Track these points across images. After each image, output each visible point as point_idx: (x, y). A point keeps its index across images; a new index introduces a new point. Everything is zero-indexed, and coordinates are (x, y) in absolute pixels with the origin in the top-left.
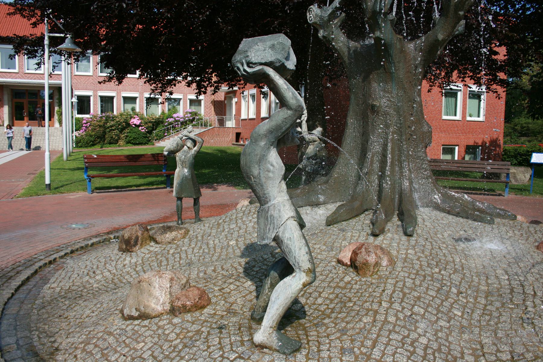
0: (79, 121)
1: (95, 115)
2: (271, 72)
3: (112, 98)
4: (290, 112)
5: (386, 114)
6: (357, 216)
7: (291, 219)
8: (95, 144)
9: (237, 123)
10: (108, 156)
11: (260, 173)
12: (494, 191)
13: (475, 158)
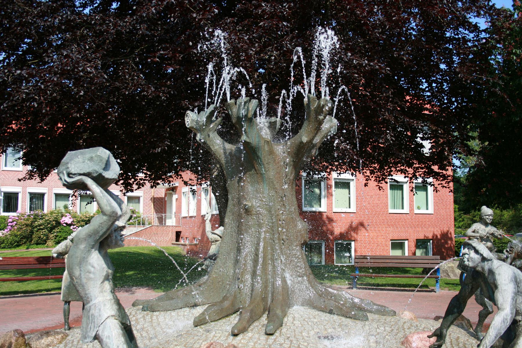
0: (5, 219)
1: (23, 213)
2: (89, 182)
3: (42, 195)
4: (105, 218)
5: (258, 214)
6: (227, 316)
7: (111, 318)
8: (21, 245)
9: (178, 221)
10: (15, 258)
11: (80, 274)
12: (426, 286)
13: (427, 253)
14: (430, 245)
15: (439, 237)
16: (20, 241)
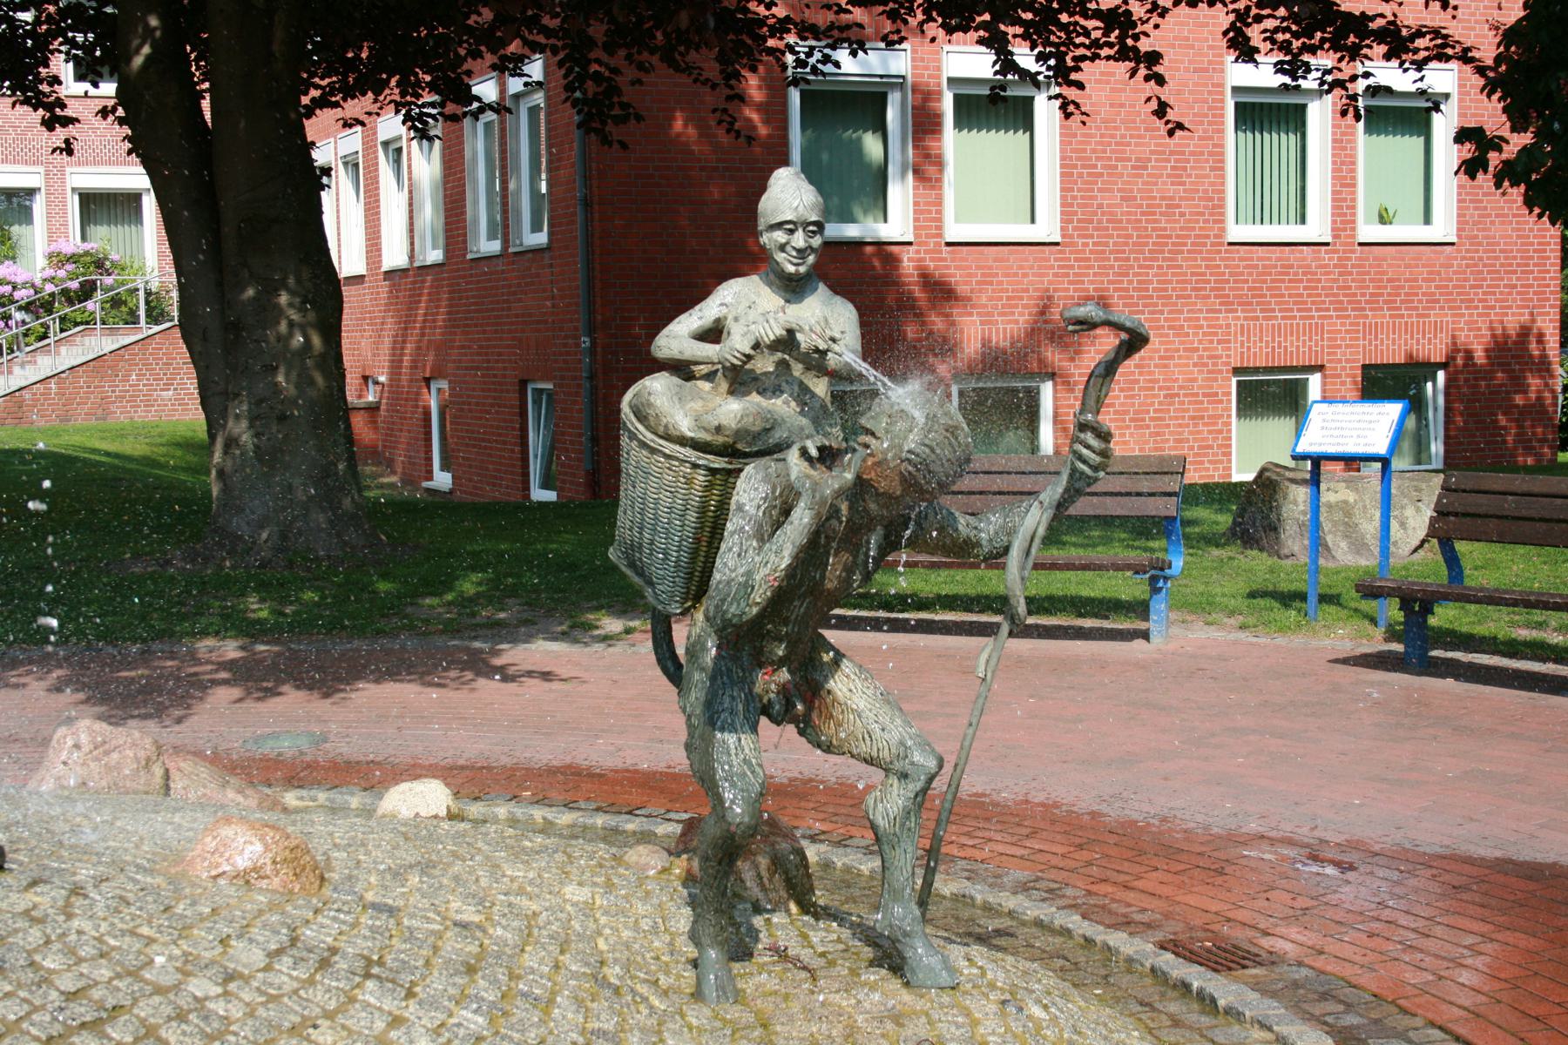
14: (1436, 388)
15: (1479, 356)
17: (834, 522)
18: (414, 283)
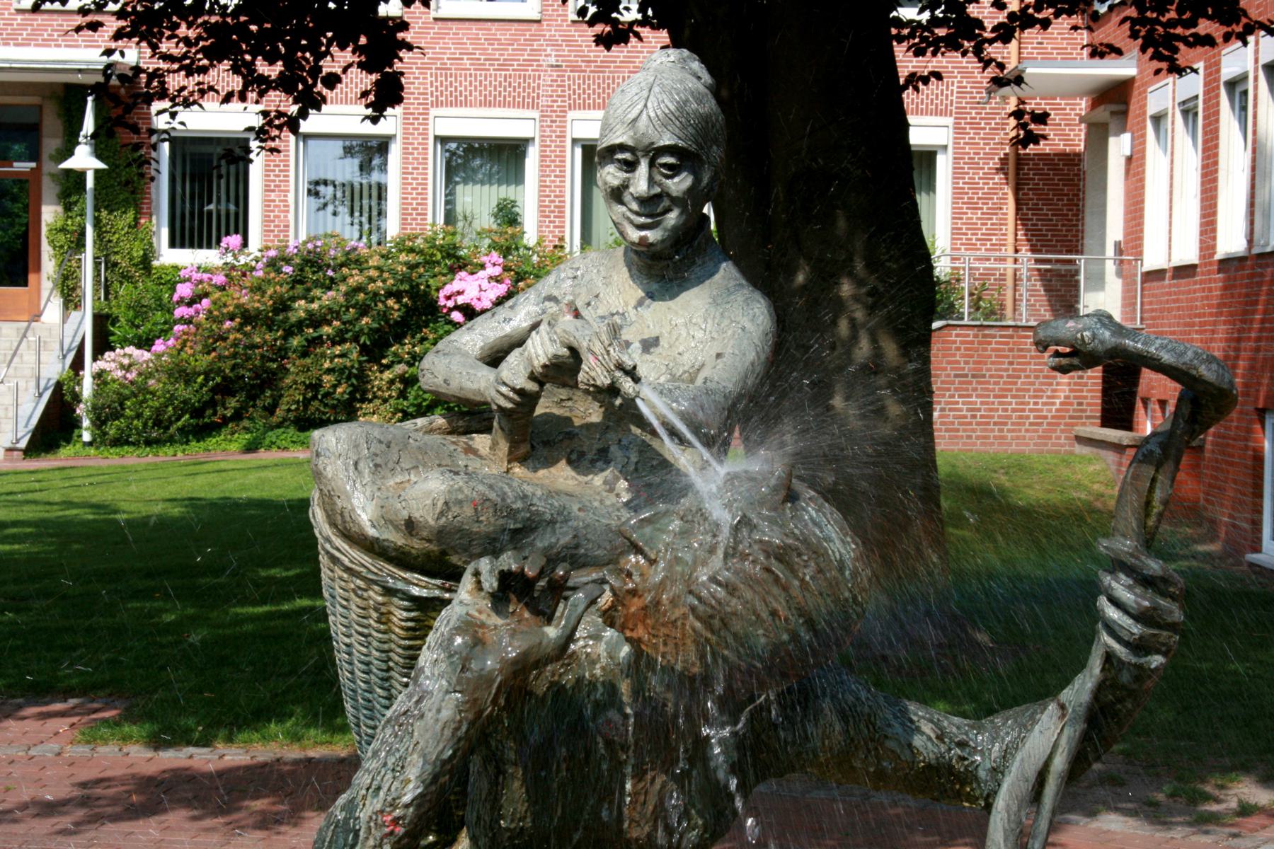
16: (212, 404)
17: (613, 714)
18: (1252, 276)
